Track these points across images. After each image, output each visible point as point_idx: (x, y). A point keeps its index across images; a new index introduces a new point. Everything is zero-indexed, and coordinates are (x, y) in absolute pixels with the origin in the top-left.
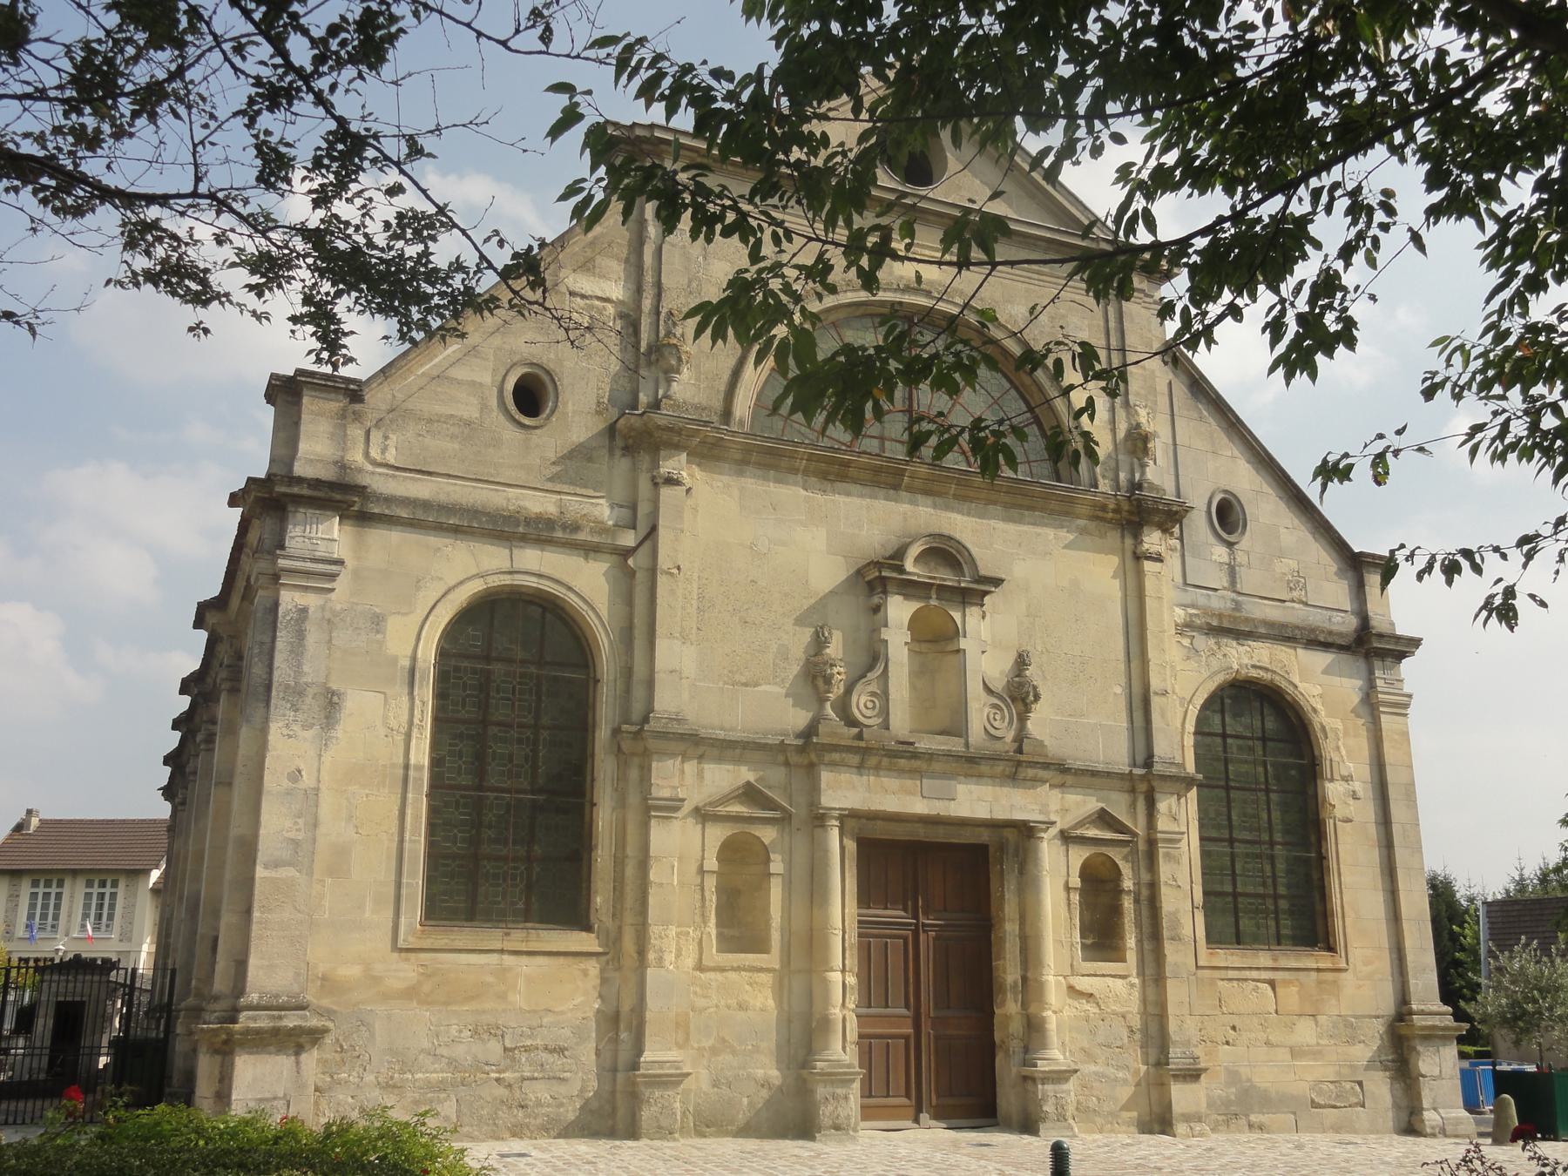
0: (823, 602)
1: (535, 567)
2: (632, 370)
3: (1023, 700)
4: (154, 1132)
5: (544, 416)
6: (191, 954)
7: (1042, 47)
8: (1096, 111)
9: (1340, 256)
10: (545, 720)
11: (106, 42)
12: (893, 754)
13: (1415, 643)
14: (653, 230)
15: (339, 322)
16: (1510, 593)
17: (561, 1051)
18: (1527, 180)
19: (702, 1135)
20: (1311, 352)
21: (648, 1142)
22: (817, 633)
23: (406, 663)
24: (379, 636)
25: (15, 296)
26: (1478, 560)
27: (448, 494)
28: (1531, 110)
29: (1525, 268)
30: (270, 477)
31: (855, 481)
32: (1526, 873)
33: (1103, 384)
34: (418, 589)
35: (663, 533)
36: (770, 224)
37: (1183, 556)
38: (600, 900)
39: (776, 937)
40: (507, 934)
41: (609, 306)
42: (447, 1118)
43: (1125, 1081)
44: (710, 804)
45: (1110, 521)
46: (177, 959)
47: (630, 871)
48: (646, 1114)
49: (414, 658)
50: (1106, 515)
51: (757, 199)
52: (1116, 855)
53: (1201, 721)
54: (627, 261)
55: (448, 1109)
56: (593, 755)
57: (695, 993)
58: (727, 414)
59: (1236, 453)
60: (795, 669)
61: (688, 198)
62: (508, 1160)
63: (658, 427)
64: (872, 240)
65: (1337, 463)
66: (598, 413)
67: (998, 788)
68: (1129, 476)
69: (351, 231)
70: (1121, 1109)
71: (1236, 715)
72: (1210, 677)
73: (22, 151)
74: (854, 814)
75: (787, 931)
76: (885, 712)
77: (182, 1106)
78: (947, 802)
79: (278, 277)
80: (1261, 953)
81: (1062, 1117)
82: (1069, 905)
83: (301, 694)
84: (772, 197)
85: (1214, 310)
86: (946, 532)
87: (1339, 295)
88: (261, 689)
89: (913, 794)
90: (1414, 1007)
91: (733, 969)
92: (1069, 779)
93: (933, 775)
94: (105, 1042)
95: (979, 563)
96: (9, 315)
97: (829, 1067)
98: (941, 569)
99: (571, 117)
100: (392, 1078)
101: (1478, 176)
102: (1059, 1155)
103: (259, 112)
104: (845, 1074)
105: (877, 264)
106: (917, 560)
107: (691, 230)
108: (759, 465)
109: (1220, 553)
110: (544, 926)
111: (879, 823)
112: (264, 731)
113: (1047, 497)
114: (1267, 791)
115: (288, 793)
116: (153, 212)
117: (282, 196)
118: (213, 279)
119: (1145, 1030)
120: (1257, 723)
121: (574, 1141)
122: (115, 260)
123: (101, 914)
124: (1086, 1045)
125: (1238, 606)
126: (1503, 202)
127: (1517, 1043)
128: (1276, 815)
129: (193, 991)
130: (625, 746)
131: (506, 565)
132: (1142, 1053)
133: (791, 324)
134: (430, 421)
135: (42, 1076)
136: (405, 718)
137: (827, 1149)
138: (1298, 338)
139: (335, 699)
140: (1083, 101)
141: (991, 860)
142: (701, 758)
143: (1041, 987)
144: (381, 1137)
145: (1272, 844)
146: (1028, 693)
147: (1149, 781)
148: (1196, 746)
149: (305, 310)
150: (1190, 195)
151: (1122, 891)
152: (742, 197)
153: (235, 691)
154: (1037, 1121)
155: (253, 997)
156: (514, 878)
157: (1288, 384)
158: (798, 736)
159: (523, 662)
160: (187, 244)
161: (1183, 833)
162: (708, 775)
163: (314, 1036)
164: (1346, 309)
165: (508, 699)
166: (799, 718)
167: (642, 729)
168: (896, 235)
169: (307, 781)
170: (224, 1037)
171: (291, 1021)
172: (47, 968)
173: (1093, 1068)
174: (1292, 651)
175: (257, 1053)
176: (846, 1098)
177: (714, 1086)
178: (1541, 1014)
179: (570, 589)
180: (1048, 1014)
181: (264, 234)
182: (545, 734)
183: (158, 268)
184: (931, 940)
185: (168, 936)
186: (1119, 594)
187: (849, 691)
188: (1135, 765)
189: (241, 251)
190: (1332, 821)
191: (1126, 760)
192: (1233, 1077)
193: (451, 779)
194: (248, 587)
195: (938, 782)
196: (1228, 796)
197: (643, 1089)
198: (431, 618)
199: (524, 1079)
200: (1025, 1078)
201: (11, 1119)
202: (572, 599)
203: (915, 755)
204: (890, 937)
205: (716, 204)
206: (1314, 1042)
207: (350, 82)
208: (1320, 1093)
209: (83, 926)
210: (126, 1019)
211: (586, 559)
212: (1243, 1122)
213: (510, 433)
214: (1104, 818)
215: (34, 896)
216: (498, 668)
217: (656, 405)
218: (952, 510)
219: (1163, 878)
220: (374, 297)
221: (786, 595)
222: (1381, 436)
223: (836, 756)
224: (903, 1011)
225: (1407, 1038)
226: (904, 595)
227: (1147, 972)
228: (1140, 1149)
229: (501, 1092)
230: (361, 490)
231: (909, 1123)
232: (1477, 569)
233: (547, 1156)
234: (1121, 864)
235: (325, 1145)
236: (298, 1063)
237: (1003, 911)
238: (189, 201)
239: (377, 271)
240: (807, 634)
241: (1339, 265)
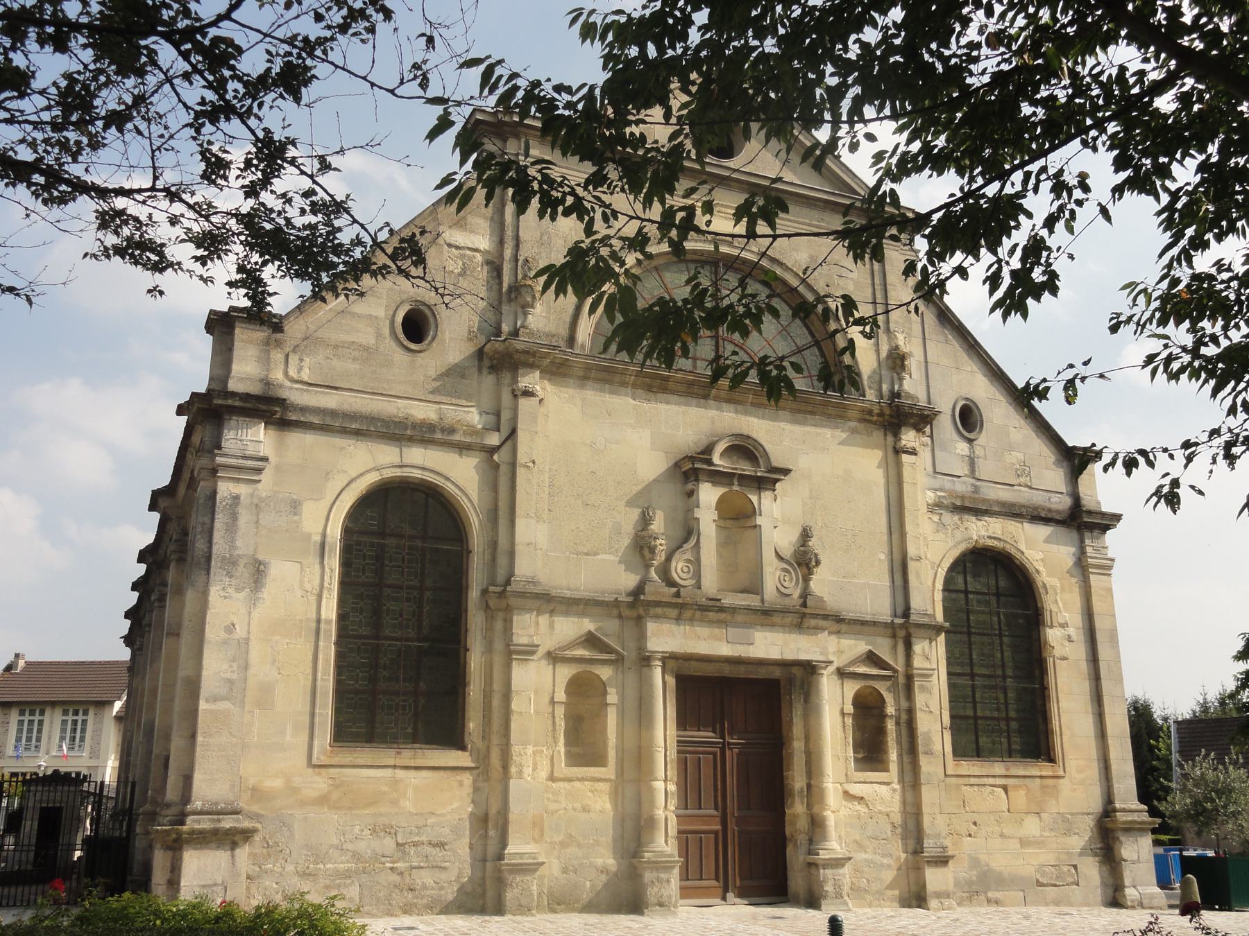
0: (648, 488)
2: (496, 308)
3: (807, 565)
4: (122, 916)
5: (426, 342)
6: (147, 768)
7: (814, 63)
8: (856, 113)
9: (1044, 226)
10: (429, 583)
11: (84, 73)
12: (704, 609)
13: (1117, 518)
14: (510, 208)
15: (265, 285)
16: (1175, 483)
17: (441, 845)
18: (1192, 163)
19: (554, 911)
20: (1023, 298)
21: (512, 917)
22: (643, 513)
23: (318, 538)
25: (15, 273)
26: (1151, 457)
27: (351, 404)
28: (1196, 107)
29: (1190, 232)
30: (210, 391)
31: (673, 392)
32: (1209, 698)
33: (861, 328)
34: (327, 479)
35: (521, 435)
36: (600, 206)
37: (933, 450)
38: (473, 725)
39: (612, 754)
40: (399, 753)
41: (478, 255)
42: (351, 900)
43: (889, 866)
44: (560, 649)
45: (875, 423)
46: (135, 774)
47: (496, 702)
48: (510, 895)
49: (324, 535)
51: (591, 188)
52: (882, 687)
53: (948, 581)
54: (492, 219)
55: (353, 892)
56: (466, 611)
57: (548, 799)
58: (571, 340)
59: (975, 368)
60: (626, 541)
61: (536, 186)
62: (400, 932)
63: (517, 351)
64: (680, 215)
65: (1037, 386)
66: (470, 339)
68: (890, 388)
69: (274, 215)
71: (975, 576)
72: (955, 546)
73: (19, 158)
74: (673, 657)
75: (621, 750)
76: (697, 575)
77: (143, 894)
79: (216, 248)
80: (996, 764)
81: (839, 895)
82: (844, 727)
84: (602, 186)
85: (946, 268)
86: (745, 432)
87: (1045, 254)
88: (203, 560)
90: (1117, 806)
91: (579, 780)
92: (844, 627)
94: (79, 841)
95: (771, 457)
96: (11, 289)
97: (654, 856)
98: (742, 462)
99: (444, 123)
100: (308, 868)
101: (1155, 161)
102: (835, 928)
103: (203, 125)
104: (667, 862)
105: (683, 237)
106: (722, 455)
107: (540, 211)
108: (597, 380)
109: (962, 447)
110: (428, 746)
111: (693, 663)
112: (205, 593)
114: (1001, 636)
115: (225, 642)
116: (120, 203)
117: (221, 189)
118: (168, 252)
120: (992, 582)
121: (451, 917)
122: (91, 238)
123: (75, 736)
124: (858, 838)
125: (976, 490)
126: (1174, 180)
127: (1199, 833)
128: (1007, 654)
129: (149, 799)
130: (492, 603)
131: (397, 460)
132: (903, 844)
133: (617, 283)
134: (336, 347)
135: (30, 867)
136: (317, 582)
137: (653, 922)
138: (1011, 289)
139: (262, 567)
140: (846, 105)
141: (782, 691)
142: (552, 612)
143: (822, 793)
144: (300, 916)
145: (1004, 677)
146: (811, 559)
147: (907, 628)
148: (944, 600)
149: (239, 276)
150: (930, 176)
152: (578, 185)
153: (182, 560)
154: (819, 899)
155: (197, 804)
156: (404, 708)
157: (1004, 321)
158: (629, 594)
159: (411, 538)
160: (147, 225)
161: (934, 670)
163: (246, 835)
164: (1051, 265)
165: (400, 567)
166: (630, 580)
167: (505, 590)
168: (699, 211)
169: (240, 632)
170: (174, 836)
171: (227, 823)
172: (33, 781)
173: (863, 856)
175: (201, 848)
176: (668, 881)
177: (563, 872)
178: (1218, 811)
179: (448, 479)
180: (828, 813)
181: (207, 218)
182: (428, 594)
183: (125, 243)
184: (735, 755)
185: (129, 755)
186: (882, 481)
187: (669, 559)
188: (895, 616)
189: (189, 230)
192: (975, 862)
193: (355, 630)
194: (192, 478)
196: (970, 640)
197: (506, 874)
198: (337, 503)
199: (412, 868)
200: (810, 865)
201: (11, 904)
202: (450, 487)
203: (722, 609)
204: (690, 753)
205: (558, 191)
206: (1037, 833)
207: (274, 100)
208: (1044, 874)
209: (61, 746)
210: (96, 821)
211: (460, 454)
212: (983, 897)
213: (400, 356)
214: (871, 658)
215: (21, 722)
216: (391, 542)
217: (515, 333)
218: (750, 414)
219: (918, 706)
220: (292, 265)
222: (1071, 366)
223: (659, 610)
224: (713, 812)
225: (1113, 831)
226: (712, 482)
228: (900, 921)
229: (395, 878)
230: (282, 402)
231: (718, 901)
232: (1151, 464)
233: (431, 929)
234: (885, 694)
235: (256, 923)
236: (233, 856)
237: (792, 731)
238: (149, 194)
239: (295, 245)
240: (635, 514)
241: (1044, 233)
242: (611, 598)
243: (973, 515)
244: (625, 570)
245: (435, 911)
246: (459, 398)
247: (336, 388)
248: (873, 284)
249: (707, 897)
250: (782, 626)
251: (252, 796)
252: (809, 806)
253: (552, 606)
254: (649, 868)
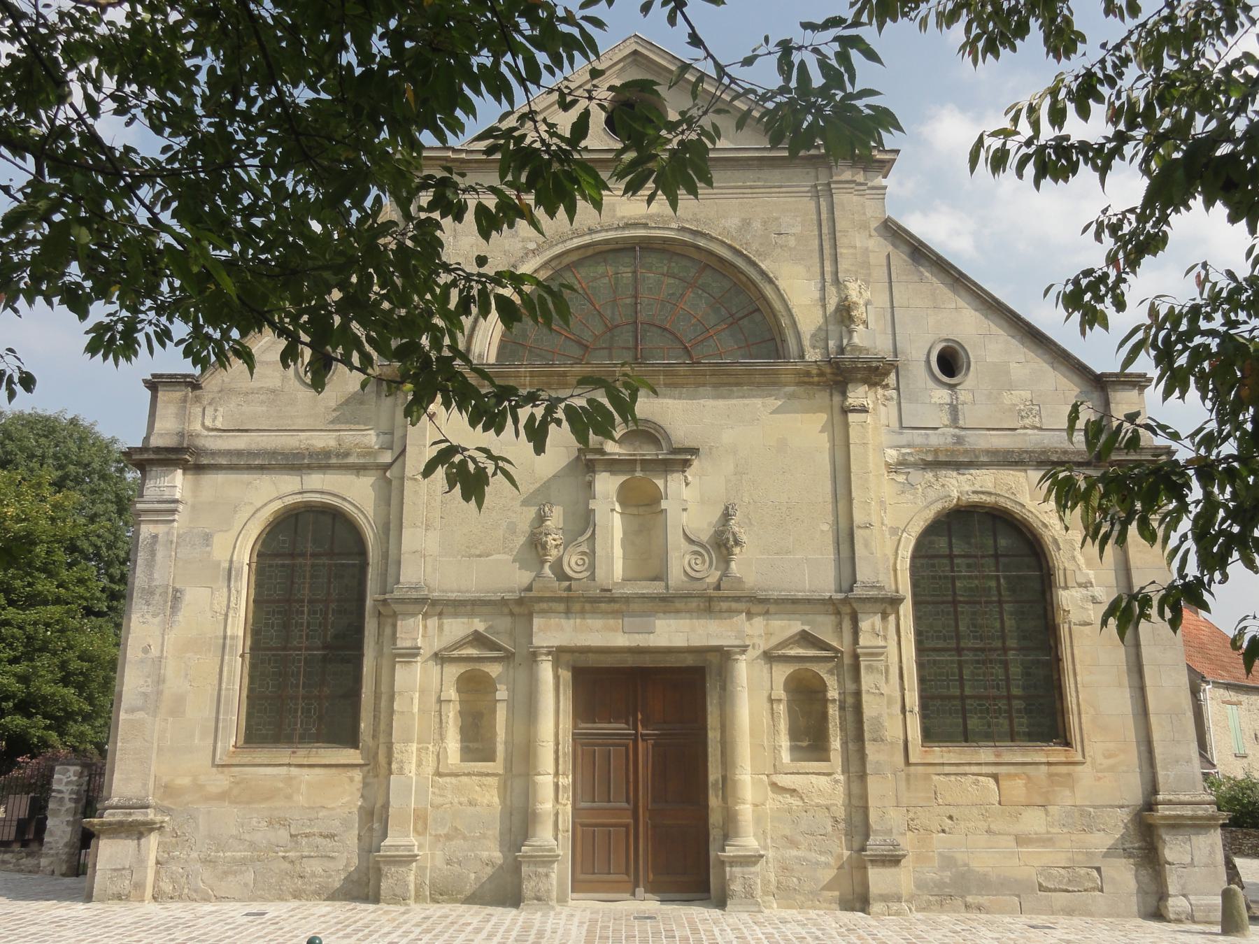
1: (318, 487)
3: (725, 545)
17: (332, 836)
23: (227, 565)
24: (208, 549)
34: (235, 512)
37: (899, 404)
43: (827, 865)
44: (445, 649)
45: (818, 384)
47: (383, 704)
49: (231, 561)
50: (811, 380)
52: (822, 670)
68: (838, 343)
70: (823, 889)
80: (982, 750)
81: (750, 895)
82: (772, 714)
83: (152, 593)
92: (772, 608)
93: (633, 614)
95: (673, 438)
109: (942, 395)
111: (590, 655)
113: (750, 373)
114: (1000, 602)
115: (142, 661)
119: (849, 820)
124: (787, 832)
125: (959, 440)
128: (1009, 623)
131: (297, 488)
134: (247, 394)
142: (440, 615)
145: (1005, 650)
146: (728, 539)
151: (828, 700)
159: (313, 555)
162: (446, 627)
169: (155, 652)
171: (138, 816)
173: (794, 853)
174: (1023, 474)
175: (113, 838)
176: (547, 875)
177: (448, 864)
179: (344, 499)
190: (1066, 626)
191: (833, 587)
195: (637, 620)
199: (303, 857)
202: (347, 507)
203: (613, 600)
206: (1043, 830)
208: (1049, 877)
211: (358, 475)
212: (959, 902)
223: (544, 606)
224: (625, 805)
226: (610, 471)
227: (852, 769)
229: (286, 866)
231: (627, 896)
234: (825, 677)
236: (139, 845)
240: (532, 512)
242: (498, 596)
243: (953, 470)
245: (323, 897)
246: (359, 424)
247: (246, 431)
248: (820, 235)
249: (618, 891)
250: (689, 612)
251: (164, 792)
252: (724, 798)
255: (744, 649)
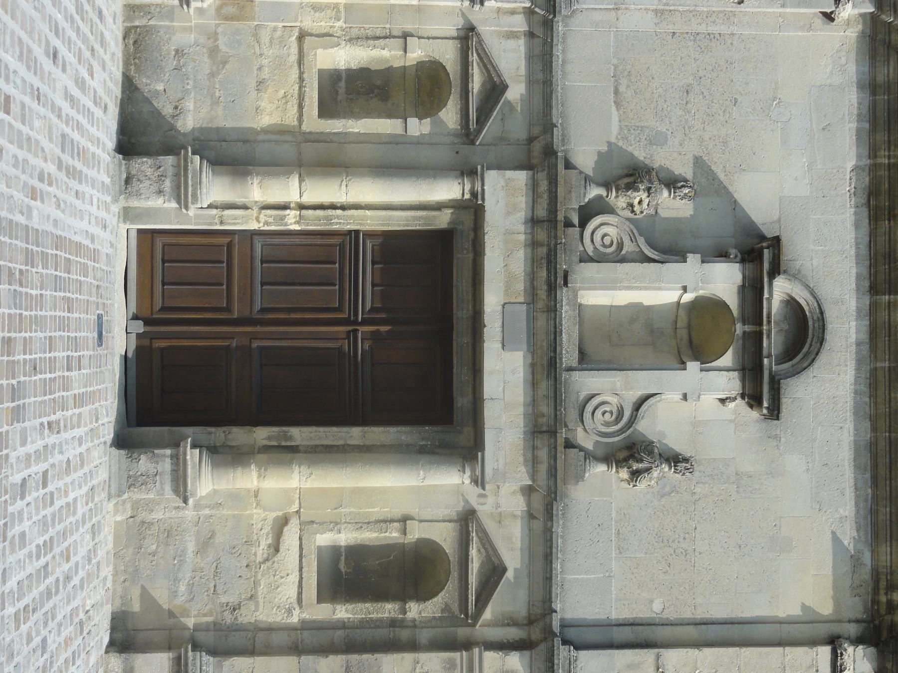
3: (632, 456)
39: (336, 126)
43: (174, 594)
44: (480, 42)
45: (875, 602)
50: (882, 592)
60: (640, 154)
67: (521, 410)
70: (143, 587)
75: (344, 138)
78: (499, 337)
89: (506, 293)
92: (538, 525)
93: (531, 319)
97: (194, 170)
119: (237, 628)
124: (219, 539)
132: (208, 623)
142: (531, 35)
162: (511, 44)
173: (191, 547)
176: (160, 192)
177: (177, 51)
186: (782, 612)
195: (523, 325)
203: (552, 288)
218: (858, 369)
221: (725, 143)
223: (544, 186)
224: (258, 306)
227: (306, 634)
231: (133, 308)
240: (683, 168)
244: (600, 154)
252: (266, 449)
253: (539, 32)
254: (179, 160)
255: (479, 481)
